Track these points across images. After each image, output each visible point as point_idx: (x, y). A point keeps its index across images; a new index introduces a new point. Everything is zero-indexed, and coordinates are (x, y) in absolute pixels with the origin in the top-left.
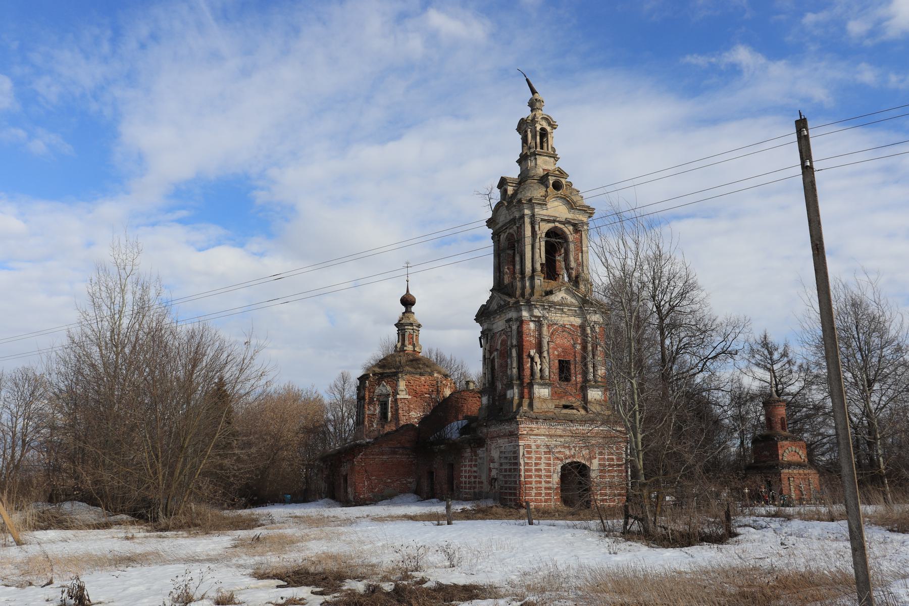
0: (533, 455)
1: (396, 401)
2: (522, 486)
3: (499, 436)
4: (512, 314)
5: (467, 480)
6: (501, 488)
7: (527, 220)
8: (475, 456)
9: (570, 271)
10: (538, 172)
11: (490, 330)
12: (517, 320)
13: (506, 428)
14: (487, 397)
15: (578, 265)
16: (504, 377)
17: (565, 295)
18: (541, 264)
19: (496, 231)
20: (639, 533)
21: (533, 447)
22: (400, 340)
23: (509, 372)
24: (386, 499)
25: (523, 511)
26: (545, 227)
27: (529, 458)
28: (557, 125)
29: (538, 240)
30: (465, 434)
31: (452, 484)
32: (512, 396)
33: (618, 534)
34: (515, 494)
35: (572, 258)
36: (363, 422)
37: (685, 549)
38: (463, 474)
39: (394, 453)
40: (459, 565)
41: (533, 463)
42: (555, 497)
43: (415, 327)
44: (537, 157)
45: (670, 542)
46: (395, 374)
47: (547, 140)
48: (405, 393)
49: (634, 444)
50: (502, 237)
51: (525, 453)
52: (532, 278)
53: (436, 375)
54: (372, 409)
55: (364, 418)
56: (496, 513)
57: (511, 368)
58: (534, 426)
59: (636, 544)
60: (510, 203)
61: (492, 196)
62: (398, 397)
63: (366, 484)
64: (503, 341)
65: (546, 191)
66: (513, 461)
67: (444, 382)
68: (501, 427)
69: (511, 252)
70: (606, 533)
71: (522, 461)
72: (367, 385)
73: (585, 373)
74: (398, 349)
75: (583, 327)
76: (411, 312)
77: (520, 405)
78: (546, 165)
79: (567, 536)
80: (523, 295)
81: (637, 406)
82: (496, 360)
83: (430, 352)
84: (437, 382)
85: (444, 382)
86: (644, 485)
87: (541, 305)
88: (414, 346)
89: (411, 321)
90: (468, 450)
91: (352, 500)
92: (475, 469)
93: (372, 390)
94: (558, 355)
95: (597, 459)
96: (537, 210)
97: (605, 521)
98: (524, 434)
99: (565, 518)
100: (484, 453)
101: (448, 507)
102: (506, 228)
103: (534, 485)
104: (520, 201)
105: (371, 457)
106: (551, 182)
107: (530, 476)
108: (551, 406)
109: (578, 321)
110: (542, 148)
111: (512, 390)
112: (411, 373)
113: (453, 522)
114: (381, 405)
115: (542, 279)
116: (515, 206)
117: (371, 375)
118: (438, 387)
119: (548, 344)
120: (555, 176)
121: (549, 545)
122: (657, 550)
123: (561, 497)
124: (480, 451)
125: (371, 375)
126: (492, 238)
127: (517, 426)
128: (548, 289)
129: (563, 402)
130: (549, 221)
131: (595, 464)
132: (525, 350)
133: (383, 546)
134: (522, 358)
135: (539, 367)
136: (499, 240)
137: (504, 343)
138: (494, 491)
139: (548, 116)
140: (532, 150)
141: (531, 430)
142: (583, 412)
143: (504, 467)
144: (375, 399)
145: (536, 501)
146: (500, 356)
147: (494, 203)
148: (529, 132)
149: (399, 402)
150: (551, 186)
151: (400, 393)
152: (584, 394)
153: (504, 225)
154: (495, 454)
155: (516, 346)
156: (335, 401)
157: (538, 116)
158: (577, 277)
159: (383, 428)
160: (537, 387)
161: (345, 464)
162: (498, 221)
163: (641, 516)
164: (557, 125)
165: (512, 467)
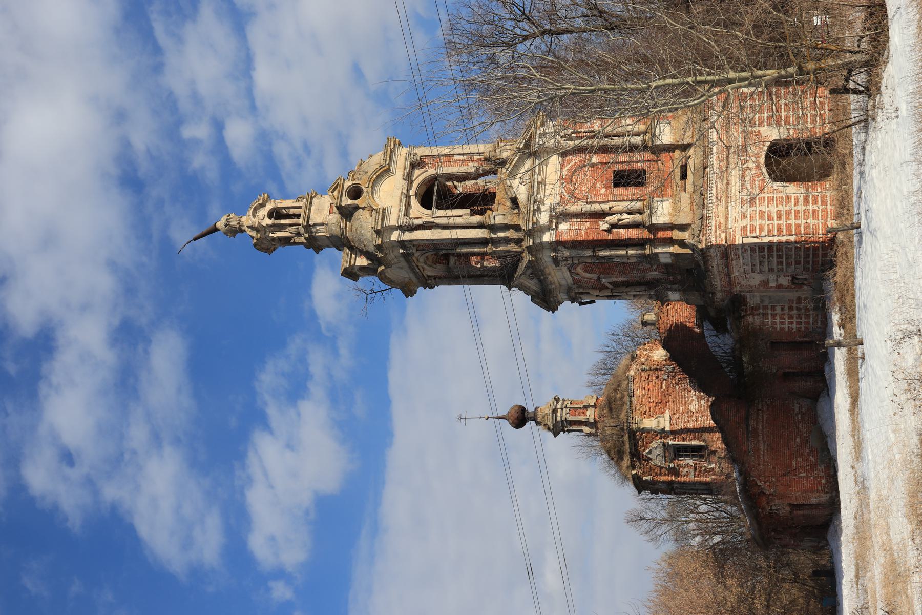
0: (757, 223)
1: (674, 433)
3: (728, 275)
4: (547, 256)
5: (794, 320)
6: (806, 269)
7: (407, 236)
8: (759, 309)
10: (334, 221)
11: (569, 290)
13: (715, 263)
14: (670, 293)
16: (641, 267)
18: (472, 215)
20: (869, 74)
22: (579, 428)
23: (633, 260)
24: (826, 444)
25: (840, 236)
26: (419, 212)
27: (761, 229)
29: (437, 221)
30: (726, 325)
31: (801, 343)
32: (668, 255)
33: (871, 103)
34: (815, 249)
36: (706, 483)
37: (890, 13)
38: (786, 326)
39: (755, 431)
40: (917, 323)
42: (819, 190)
43: (559, 406)
44: (311, 223)
45: (880, 33)
46: (632, 434)
47: (285, 208)
48: (661, 419)
49: (742, 83)
50: (429, 274)
51: (754, 235)
52: (493, 228)
53: (632, 373)
54: (686, 469)
55: (700, 483)
56: (845, 276)
57: (627, 256)
59: (885, 80)
60: (379, 262)
61: (368, 288)
62: (668, 429)
63: (804, 475)
64: (586, 270)
65: (363, 208)
66: (766, 253)
67: (643, 360)
68: (715, 270)
69: (452, 260)
70: (870, 119)
71: (766, 240)
72: (649, 478)
73: (633, 148)
74: (593, 431)
75: (564, 154)
76: (535, 412)
77: (682, 244)
78: (323, 209)
79: (874, 175)
80: (519, 242)
81: (690, 79)
82: (614, 279)
83: (592, 384)
84: (643, 370)
85: (643, 360)
86: (800, 68)
87: (534, 215)
88: (587, 407)
89: (548, 411)
90: (750, 319)
91: (829, 495)
92: (778, 310)
93: (658, 471)
95: (762, 129)
96: (393, 221)
97: (853, 121)
98: (726, 238)
99: (849, 177)
100: (754, 296)
101: (839, 345)
102: (418, 266)
103: (802, 221)
104: (379, 248)
106: (350, 202)
107: (788, 227)
108: (685, 198)
109: (554, 160)
110: (298, 216)
111: (660, 256)
112: (630, 411)
113: (859, 336)
114: (680, 456)
117: (634, 472)
118: (651, 370)
119: (590, 203)
120: (341, 196)
121: (888, 201)
122: (891, 53)
123: (818, 181)
124: (752, 302)
125: (634, 472)
126: (431, 287)
127: (713, 247)
128: (509, 204)
130: (408, 205)
131: (772, 134)
132: (600, 238)
133: (894, 431)
134: (612, 241)
135: (625, 216)
136: (435, 278)
137: (588, 269)
138: (811, 281)
140: (302, 230)
141: (720, 226)
142: (691, 151)
143: (775, 266)
145: (825, 218)
146: (608, 274)
147: (379, 285)
148: (275, 235)
149: (676, 428)
150: (356, 202)
151: (661, 427)
153: (412, 269)
154: (756, 279)
155: (594, 251)
156: (672, 533)
157: (250, 223)
159: (714, 452)
161: (774, 508)
162: (407, 280)
163: (845, 73)
165: (775, 254)
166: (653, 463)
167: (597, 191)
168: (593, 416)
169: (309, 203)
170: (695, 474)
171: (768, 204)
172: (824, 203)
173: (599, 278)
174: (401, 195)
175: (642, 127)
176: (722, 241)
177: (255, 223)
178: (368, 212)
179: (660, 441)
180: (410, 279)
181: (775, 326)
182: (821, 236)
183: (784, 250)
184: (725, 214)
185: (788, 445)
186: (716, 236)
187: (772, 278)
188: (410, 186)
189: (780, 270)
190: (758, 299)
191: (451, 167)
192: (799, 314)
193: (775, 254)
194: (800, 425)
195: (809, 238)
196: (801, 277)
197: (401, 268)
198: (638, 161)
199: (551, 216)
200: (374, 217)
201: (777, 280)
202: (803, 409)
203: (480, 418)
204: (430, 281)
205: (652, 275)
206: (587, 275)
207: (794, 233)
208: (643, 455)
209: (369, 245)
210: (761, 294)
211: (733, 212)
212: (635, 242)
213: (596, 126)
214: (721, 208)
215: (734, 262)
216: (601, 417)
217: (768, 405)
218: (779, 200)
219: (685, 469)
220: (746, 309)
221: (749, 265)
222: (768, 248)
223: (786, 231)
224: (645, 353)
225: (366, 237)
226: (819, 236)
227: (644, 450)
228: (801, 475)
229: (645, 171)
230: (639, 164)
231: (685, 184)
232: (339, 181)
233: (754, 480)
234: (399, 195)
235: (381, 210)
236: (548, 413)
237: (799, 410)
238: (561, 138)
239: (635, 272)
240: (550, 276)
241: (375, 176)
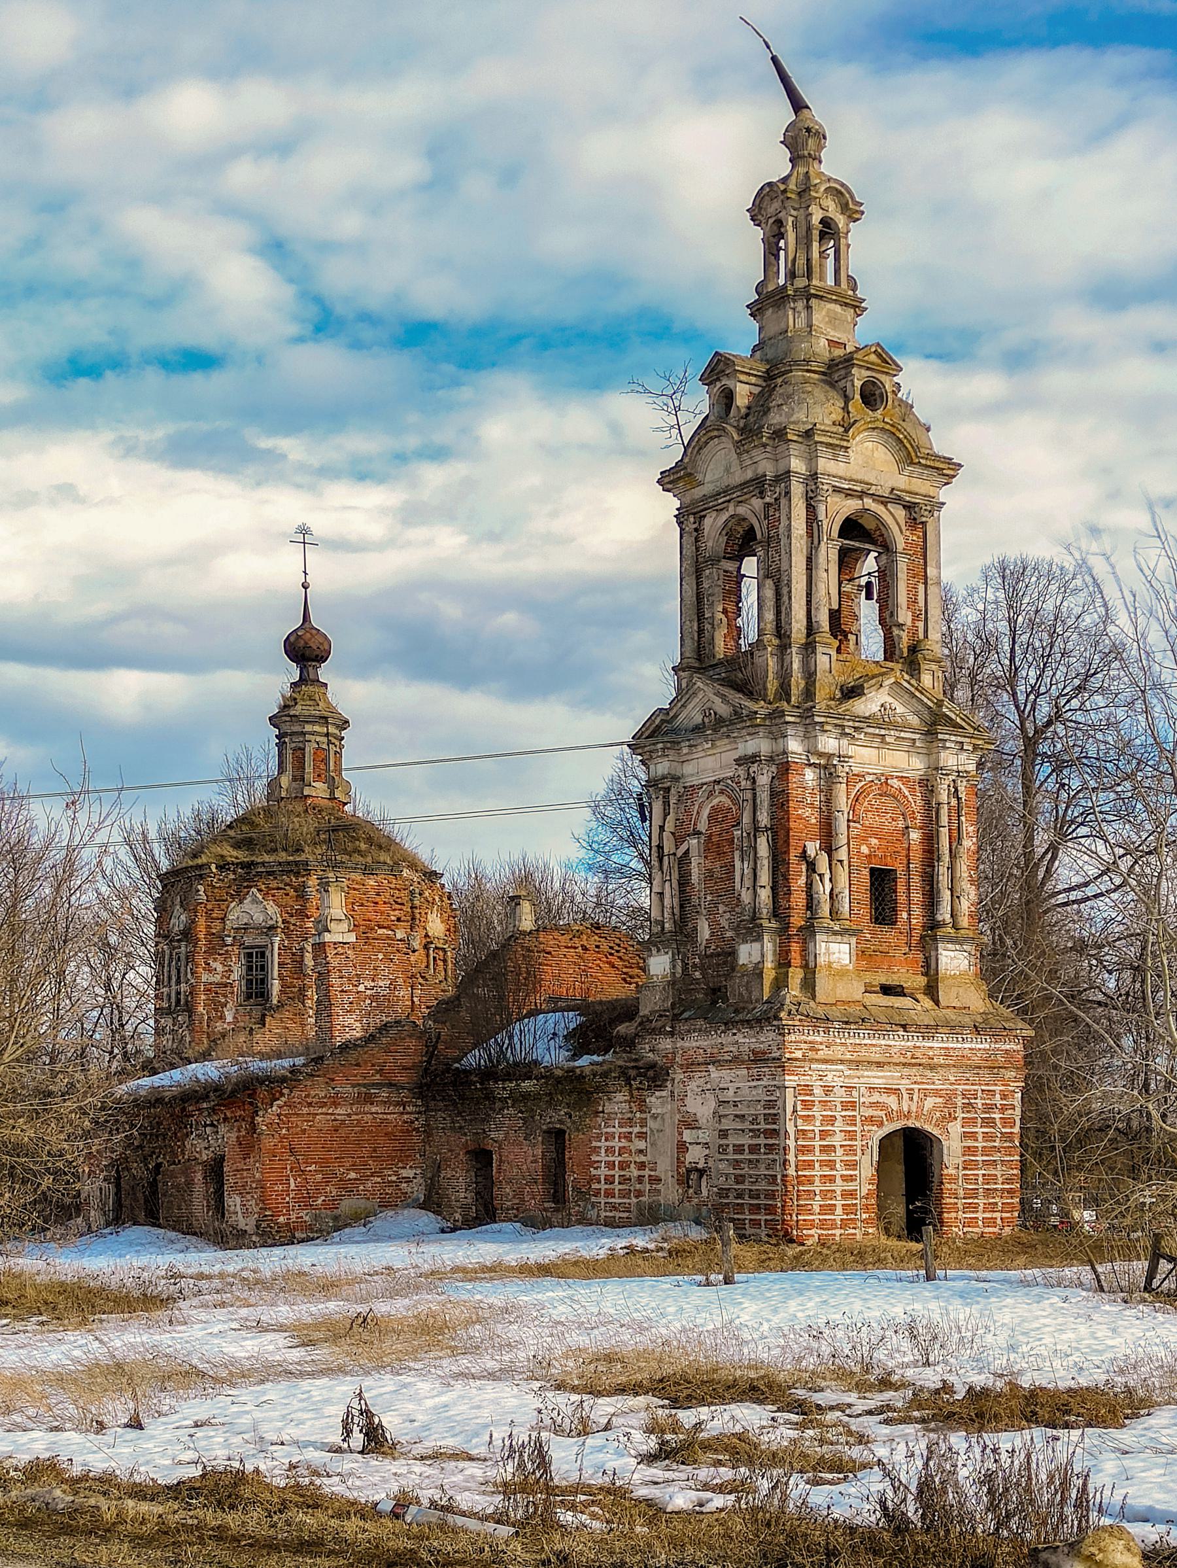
0: (817, 1112)
2: (790, 1188)
4: (761, 745)
5: (617, 1173)
9: (896, 631)
12: (771, 759)
13: (745, 1041)
15: (916, 618)
17: (891, 700)
19: (694, 503)
21: (818, 1091)
25: (791, 1251)
28: (863, 213)
32: (756, 958)
34: (770, 1210)
35: (902, 598)
39: (369, 1099)
41: (817, 1132)
43: (332, 730)
44: (814, 302)
48: (344, 926)
50: (708, 522)
52: (809, 647)
53: (406, 873)
58: (819, 1039)
63: (292, 1186)
65: (845, 409)
66: (763, 1126)
68: (727, 1039)
71: (791, 1129)
75: (927, 786)
77: (780, 983)
80: (784, 691)
82: (694, 862)
88: (332, 785)
92: (641, 1145)
94: (869, 856)
95: (959, 1122)
98: (796, 1059)
100: (663, 1104)
102: (729, 501)
103: (817, 1187)
104: (780, 434)
105: (305, 1110)
106: (858, 384)
107: (810, 1165)
109: (916, 765)
113: (737, 1277)
115: (833, 653)
116: (764, 445)
120: (868, 369)
124: (653, 1099)
125: (213, 867)
129: (883, 979)
130: (849, 494)
139: (843, 185)
140: (801, 283)
142: (927, 1003)
143: (732, 1140)
144: (229, 940)
145: (823, 1224)
149: (330, 952)
150: (857, 397)
151: (332, 926)
152: (927, 960)
154: (702, 1108)
158: (914, 649)
160: (824, 937)
162: (700, 477)
164: (863, 213)
165: (762, 1141)
166: (232, 905)
167: (865, 839)
168: (314, 794)
169: (848, 301)
170: (211, 984)
171: (845, 1131)
172: (844, 1224)
173: (697, 833)
174: (867, 484)
175: (964, 922)
176: (790, 1053)
177: (817, 192)
178: (840, 418)
179: (280, 920)
180: (701, 484)
181: (603, 1138)
182: (795, 1218)
183: (770, 1156)
184: (831, 1058)
185: (343, 1158)
186: (798, 1042)
187: (701, 1135)
188: (878, 501)
189: (723, 1149)
190: (659, 1111)
191: (906, 578)
192: (630, 1180)
193: (762, 1141)
194: (379, 1180)
195: (791, 1199)
196: (704, 1184)
197: (727, 470)
198: (912, 915)
199: (830, 756)
200: (832, 430)
201: (698, 1144)
202: (406, 1185)
203: (305, 572)
204: (692, 520)
205: (703, 927)
206: (705, 813)
207: (800, 1173)
208: (251, 887)
209: (781, 415)
210: (667, 1116)
211: (834, 1073)
212: (783, 903)
213: (968, 843)
214: (840, 1053)
215: (745, 1072)
216: (314, 809)
217: (412, 1122)
218: (851, 1150)
219: (221, 966)
220: (643, 1089)
221: (735, 1097)
222: (775, 1130)
223: (804, 1161)
224: (437, 898)
225: (796, 409)
226: (794, 1216)
227: (260, 890)
228: (292, 1180)
229: (894, 923)
230: (905, 915)
231: (875, 992)
232: (894, 367)
233: (282, 1095)
234: (866, 479)
235: (845, 444)
236: (320, 708)
237: (403, 1178)
238: (954, 781)
239: (709, 898)
240: (710, 745)
241: (901, 436)
